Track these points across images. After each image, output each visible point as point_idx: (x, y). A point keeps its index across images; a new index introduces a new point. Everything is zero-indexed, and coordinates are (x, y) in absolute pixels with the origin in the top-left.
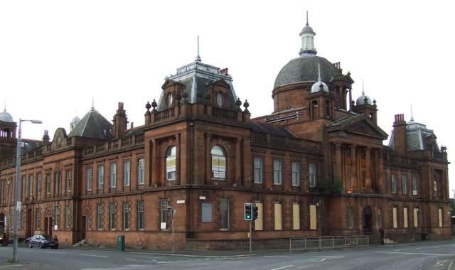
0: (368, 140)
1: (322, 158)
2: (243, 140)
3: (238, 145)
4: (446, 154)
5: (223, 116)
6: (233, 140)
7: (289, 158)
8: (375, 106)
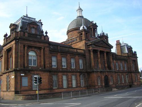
0: (105, 49)
1: (85, 56)
2: (44, 48)
3: (42, 51)
4: (136, 54)
5: (32, 37)
6: (40, 48)
7: (69, 56)
8: (107, 36)
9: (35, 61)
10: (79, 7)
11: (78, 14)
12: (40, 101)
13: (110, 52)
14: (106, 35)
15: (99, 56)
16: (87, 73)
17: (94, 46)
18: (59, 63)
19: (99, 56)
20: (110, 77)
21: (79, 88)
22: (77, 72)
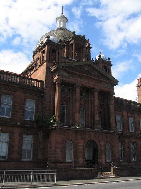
9: (8, 110)
10: (62, 14)
11: (59, 25)
12: (34, 183)
13: (109, 92)
14: (107, 60)
15: (78, 95)
16: (41, 128)
17: (66, 74)
18: (125, 124)
19: (78, 95)
20: (101, 144)
21: (14, 163)
22: (14, 126)
